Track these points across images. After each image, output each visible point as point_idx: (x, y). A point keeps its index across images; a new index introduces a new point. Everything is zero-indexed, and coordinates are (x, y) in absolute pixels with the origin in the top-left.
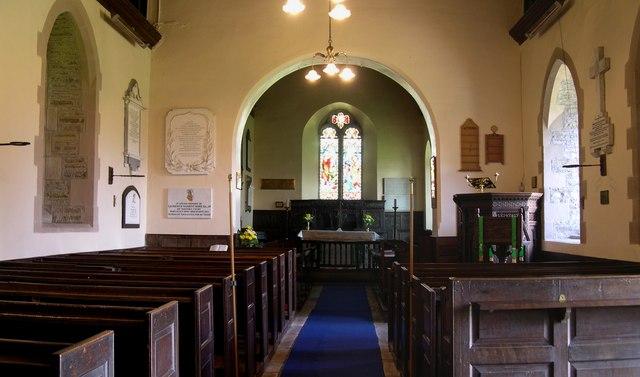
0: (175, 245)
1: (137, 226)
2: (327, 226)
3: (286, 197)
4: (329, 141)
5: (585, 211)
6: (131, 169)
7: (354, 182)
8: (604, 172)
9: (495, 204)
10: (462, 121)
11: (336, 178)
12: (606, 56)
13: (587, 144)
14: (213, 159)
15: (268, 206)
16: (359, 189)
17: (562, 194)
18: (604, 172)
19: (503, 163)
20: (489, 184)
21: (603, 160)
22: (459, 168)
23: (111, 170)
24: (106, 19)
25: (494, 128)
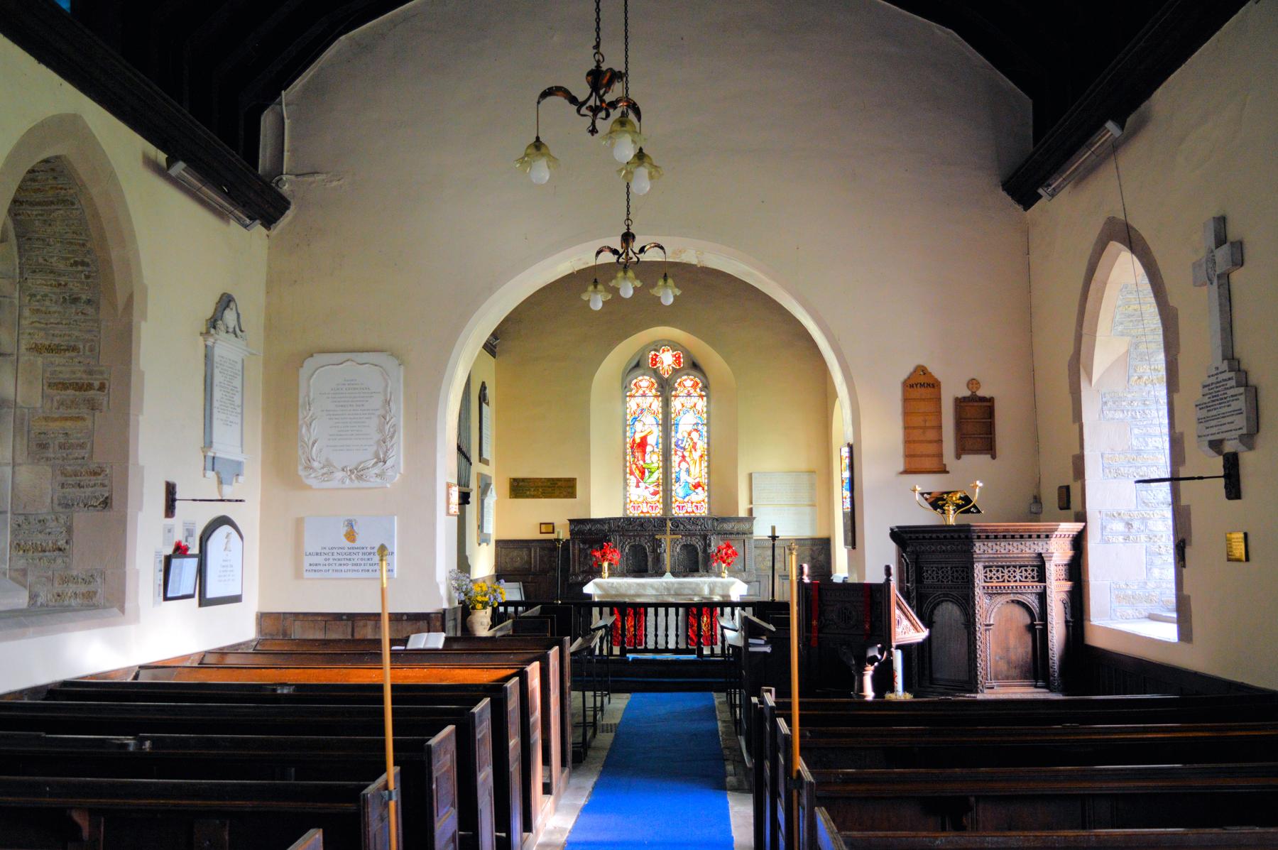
0: (319, 635)
1: (236, 599)
2: (640, 571)
4: (645, 403)
6: (220, 482)
7: (692, 481)
8: (1233, 489)
9: (979, 547)
10: (905, 371)
11: (658, 475)
12: (1232, 236)
13: (1190, 430)
14: (398, 456)
15: (527, 531)
16: (701, 495)
17: (1129, 525)
18: (1233, 489)
19: (994, 457)
20: (966, 505)
22: (901, 468)
23: (171, 490)
24: (162, 172)
25: (973, 383)
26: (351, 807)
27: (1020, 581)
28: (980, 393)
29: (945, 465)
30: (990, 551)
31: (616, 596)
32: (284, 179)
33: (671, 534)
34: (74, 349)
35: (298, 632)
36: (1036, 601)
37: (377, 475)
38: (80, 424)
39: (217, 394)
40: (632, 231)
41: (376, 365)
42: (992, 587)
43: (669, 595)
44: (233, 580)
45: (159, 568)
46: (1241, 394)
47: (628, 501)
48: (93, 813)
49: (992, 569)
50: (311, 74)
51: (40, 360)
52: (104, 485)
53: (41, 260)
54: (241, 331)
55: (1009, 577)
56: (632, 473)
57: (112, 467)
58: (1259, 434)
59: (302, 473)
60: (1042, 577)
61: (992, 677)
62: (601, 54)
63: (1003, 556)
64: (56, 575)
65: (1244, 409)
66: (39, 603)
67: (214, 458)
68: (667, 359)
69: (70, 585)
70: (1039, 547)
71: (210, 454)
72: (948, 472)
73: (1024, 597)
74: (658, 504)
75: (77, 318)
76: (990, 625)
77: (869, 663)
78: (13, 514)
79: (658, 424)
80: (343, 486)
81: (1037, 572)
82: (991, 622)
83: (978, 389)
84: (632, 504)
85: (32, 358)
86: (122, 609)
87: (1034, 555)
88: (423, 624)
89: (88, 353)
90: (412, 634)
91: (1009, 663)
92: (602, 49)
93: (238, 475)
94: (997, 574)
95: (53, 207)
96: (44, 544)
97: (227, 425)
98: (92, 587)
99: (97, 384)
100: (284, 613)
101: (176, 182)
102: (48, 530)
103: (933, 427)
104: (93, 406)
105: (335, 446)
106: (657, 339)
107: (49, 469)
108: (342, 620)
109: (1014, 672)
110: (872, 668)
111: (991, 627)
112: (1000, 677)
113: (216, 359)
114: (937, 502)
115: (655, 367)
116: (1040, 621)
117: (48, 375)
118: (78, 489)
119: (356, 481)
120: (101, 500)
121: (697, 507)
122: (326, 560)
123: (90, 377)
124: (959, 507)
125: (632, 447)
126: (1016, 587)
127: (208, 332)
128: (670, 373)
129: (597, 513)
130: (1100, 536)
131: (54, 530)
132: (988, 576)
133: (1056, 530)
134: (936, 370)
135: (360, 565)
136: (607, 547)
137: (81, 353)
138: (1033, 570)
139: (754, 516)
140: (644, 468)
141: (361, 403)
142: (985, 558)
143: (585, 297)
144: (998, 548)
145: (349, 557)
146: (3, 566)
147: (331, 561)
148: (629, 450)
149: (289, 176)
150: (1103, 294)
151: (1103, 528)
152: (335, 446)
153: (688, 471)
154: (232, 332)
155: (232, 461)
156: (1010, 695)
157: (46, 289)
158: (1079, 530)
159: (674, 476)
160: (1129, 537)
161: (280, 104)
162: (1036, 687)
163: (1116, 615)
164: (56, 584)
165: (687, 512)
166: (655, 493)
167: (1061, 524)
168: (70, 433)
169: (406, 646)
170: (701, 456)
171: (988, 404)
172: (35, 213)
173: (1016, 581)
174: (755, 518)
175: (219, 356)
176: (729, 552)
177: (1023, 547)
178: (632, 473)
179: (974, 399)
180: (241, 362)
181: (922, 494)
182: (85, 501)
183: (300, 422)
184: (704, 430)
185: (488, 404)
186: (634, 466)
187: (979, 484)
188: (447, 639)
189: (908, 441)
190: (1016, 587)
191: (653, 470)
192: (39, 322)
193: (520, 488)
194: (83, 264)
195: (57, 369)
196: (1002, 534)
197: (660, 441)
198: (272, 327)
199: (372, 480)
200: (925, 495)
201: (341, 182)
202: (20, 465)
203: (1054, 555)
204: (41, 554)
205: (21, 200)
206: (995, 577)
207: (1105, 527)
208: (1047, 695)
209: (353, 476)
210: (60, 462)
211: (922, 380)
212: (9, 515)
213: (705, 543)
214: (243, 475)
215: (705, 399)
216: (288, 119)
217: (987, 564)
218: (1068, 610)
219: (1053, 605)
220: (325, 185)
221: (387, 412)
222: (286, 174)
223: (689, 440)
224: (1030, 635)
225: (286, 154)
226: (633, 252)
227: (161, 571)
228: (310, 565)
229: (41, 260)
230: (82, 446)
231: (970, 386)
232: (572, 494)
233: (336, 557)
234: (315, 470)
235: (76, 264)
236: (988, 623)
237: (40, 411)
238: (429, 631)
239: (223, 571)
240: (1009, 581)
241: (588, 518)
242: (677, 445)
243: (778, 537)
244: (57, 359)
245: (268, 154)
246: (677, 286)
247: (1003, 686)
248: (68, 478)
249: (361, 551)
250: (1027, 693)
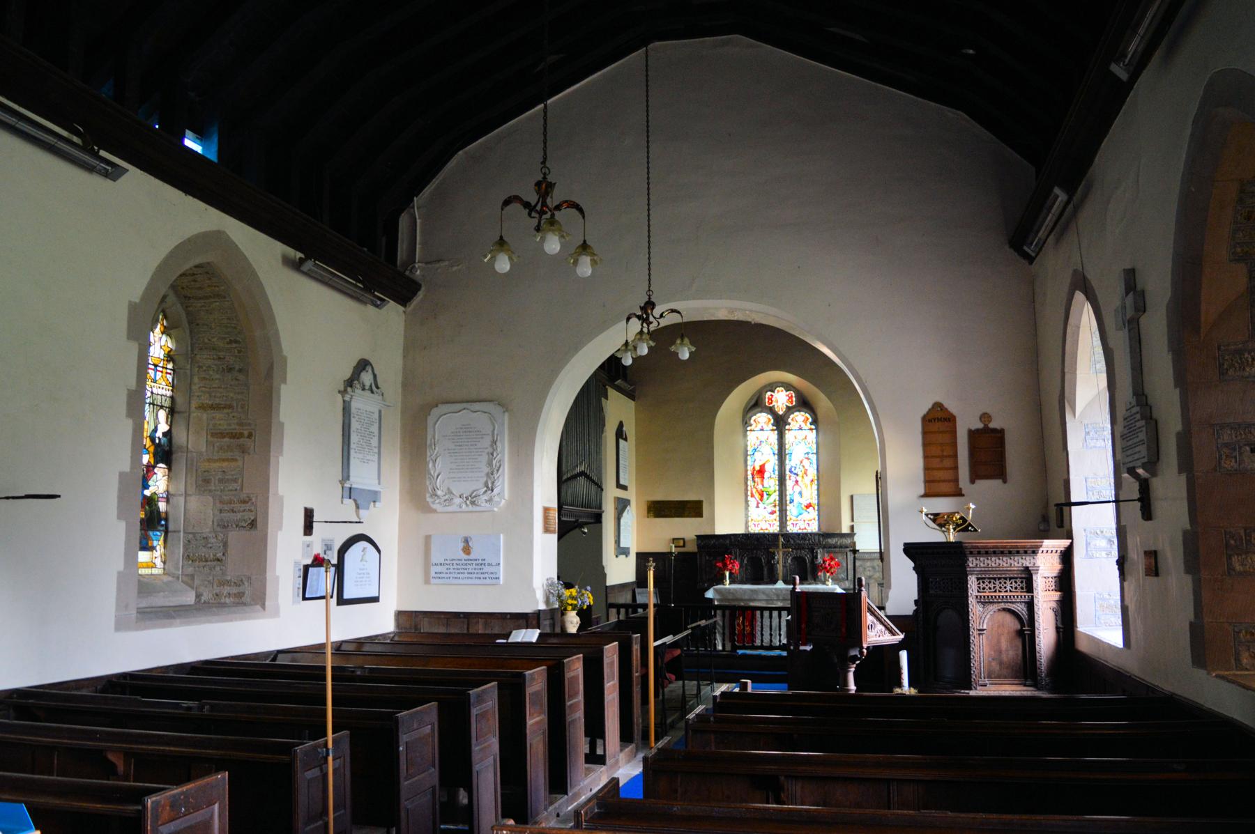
0: (442, 630)
1: (375, 600)
2: (757, 580)
3: (687, 529)
4: (762, 436)
5: (1126, 584)
6: (357, 507)
7: (805, 503)
9: (972, 562)
11: (775, 496)
16: (813, 514)
19: (1005, 482)
21: (1145, 487)
22: (922, 492)
23: (309, 514)
24: (297, 266)
25: (985, 417)
26: (285, 758)
27: (1011, 591)
28: (991, 425)
29: (961, 489)
30: (982, 565)
31: (733, 600)
32: (417, 266)
33: (783, 548)
34: (230, 407)
35: (426, 627)
36: (1025, 609)
37: (486, 501)
38: (233, 464)
39: (354, 438)
40: (653, 299)
41: (485, 412)
42: (984, 596)
43: (778, 600)
44: (370, 585)
45: (298, 575)
46: (1143, 426)
47: (750, 519)
48: (128, 755)
49: (1017, 580)
50: (437, 182)
51: (205, 416)
52: (250, 511)
53: (206, 341)
54: (378, 388)
55: (1000, 588)
56: (752, 496)
57: (257, 496)
58: (1160, 462)
59: (429, 499)
60: (1030, 588)
61: (986, 677)
62: (548, 168)
63: (994, 569)
64: (215, 579)
65: (1146, 440)
66: (203, 601)
67: (350, 488)
68: (781, 399)
69: (225, 587)
70: (1027, 561)
71: (347, 485)
72: (963, 495)
73: (1014, 605)
74: (774, 522)
75: (232, 383)
76: (983, 630)
77: (850, 662)
78: (185, 532)
79: (774, 454)
80: (460, 510)
81: (1026, 583)
82: (985, 627)
83: (990, 421)
84: (753, 522)
85: (199, 414)
86: (263, 606)
87: (1022, 569)
88: (522, 622)
89: (239, 410)
90: (514, 629)
91: (1001, 663)
92: (548, 164)
93: (374, 502)
94: (989, 585)
95: (212, 300)
96: (207, 556)
97: (364, 462)
98: (241, 589)
99: (246, 433)
100: (416, 612)
101: (308, 274)
102: (210, 545)
103: (949, 456)
104: (243, 450)
105: (454, 478)
106: (771, 381)
107: (211, 499)
108: (460, 618)
109: (1005, 672)
110: (855, 665)
111: (985, 632)
112: (993, 676)
113: (353, 410)
114: (938, 519)
115: (771, 405)
116: (1028, 627)
117: (211, 426)
118: (232, 514)
119: (470, 506)
120: (249, 522)
121: (809, 524)
122: (447, 569)
123: (241, 428)
124: (958, 525)
125: (753, 474)
126: (1006, 596)
127: (345, 391)
128: (784, 410)
129: (721, 529)
130: (1085, 552)
131: (214, 545)
132: (982, 587)
133: (1041, 546)
134: (952, 406)
135: (474, 573)
136: (727, 559)
137: (235, 410)
138: (1022, 582)
139: (855, 532)
140: (763, 492)
141: (474, 443)
142: (977, 571)
143: (673, 348)
144: (989, 562)
145: (465, 567)
146: (177, 572)
147: (452, 570)
148: (750, 477)
149: (420, 264)
150: (1078, 337)
151: (1088, 544)
152: (454, 478)
153: (800, 493)
154: (368, 390)
155: (369, 491)
156: (1000, 692)
157: (209, 362)
158: (1066, 546)
159: (788, 498)
160: (1111, 553)
161: (413, 207)
162: (1025, 685)
163: (1101, 623)
164: (215, 587)
165: (762, 529)
166: (773, 513)
167: (1045, 541)
168: (226, 471)
169: (507, 639)
170: (812, 481)
171: (999, 435)
172: (199, 305)
173: (1006, 591)
174: (855, 534)
175: (356, 409)
176: (833, 563)
177: (1012, 561)
178: (752, 496)
179: (986, 431)
180: (378, 413)
181: (927, 515)
182: (237, 523)
183: (428, 459)
184: (814, 458)
185: (626, 439)
186: (754, 490)
187: (972, 506)
188: (541, 635)
189: (927, 469)
190: (1006, 596)
191: (770, 493)
192: (205, 387)
193: (659, 509)
194: (236, 342)
195: (218, 422)
196: (992, 550)
197: (777, 468)
198: (408, 384)
199: (482, 505)
200: (929, 516)
201: (460, 267)
202: (190, 495)
203: (1040, 568)
204: (205, 563)
205: (189, 295)
206: (987, 588)
207: (1090, 544)
208: (1034, 692)
209: (468, 502)
210: (219, 493)
211: (940, 415)
212: (182, 534)
213: (813, 555)
214: (380, 502)
215: (814, 431)
216: (419, 218)
217: (980, 576)
218: (1059, 618)
219: (1040, 613)
220: (448, 270)
221: (494, 450)
222: (419, 262)
223: (801, 467)
224: (1020, 640)
225: (418, 246)
226: (653, 317)
227: (300, 577)
228: (436, 573)
229: (206, 341)
230: (235, 481)
231: (983, 419)
232: (699, 514)
233: (455, 567)
234: (438, 497)
235: (231, 342)
236: (981, 628)
237: (205, 454)
238: (527, 628)
239: (360, 578)
240: (1000, 591)
241: (712, 533)
242: (791, 472)
243: (858, 551)
244: (218, 415)
245: (405, 247)
246: (692, 343)
247: (996, 684)
248: (225, 506)
249: (475, 562)
250: (1016, 691)
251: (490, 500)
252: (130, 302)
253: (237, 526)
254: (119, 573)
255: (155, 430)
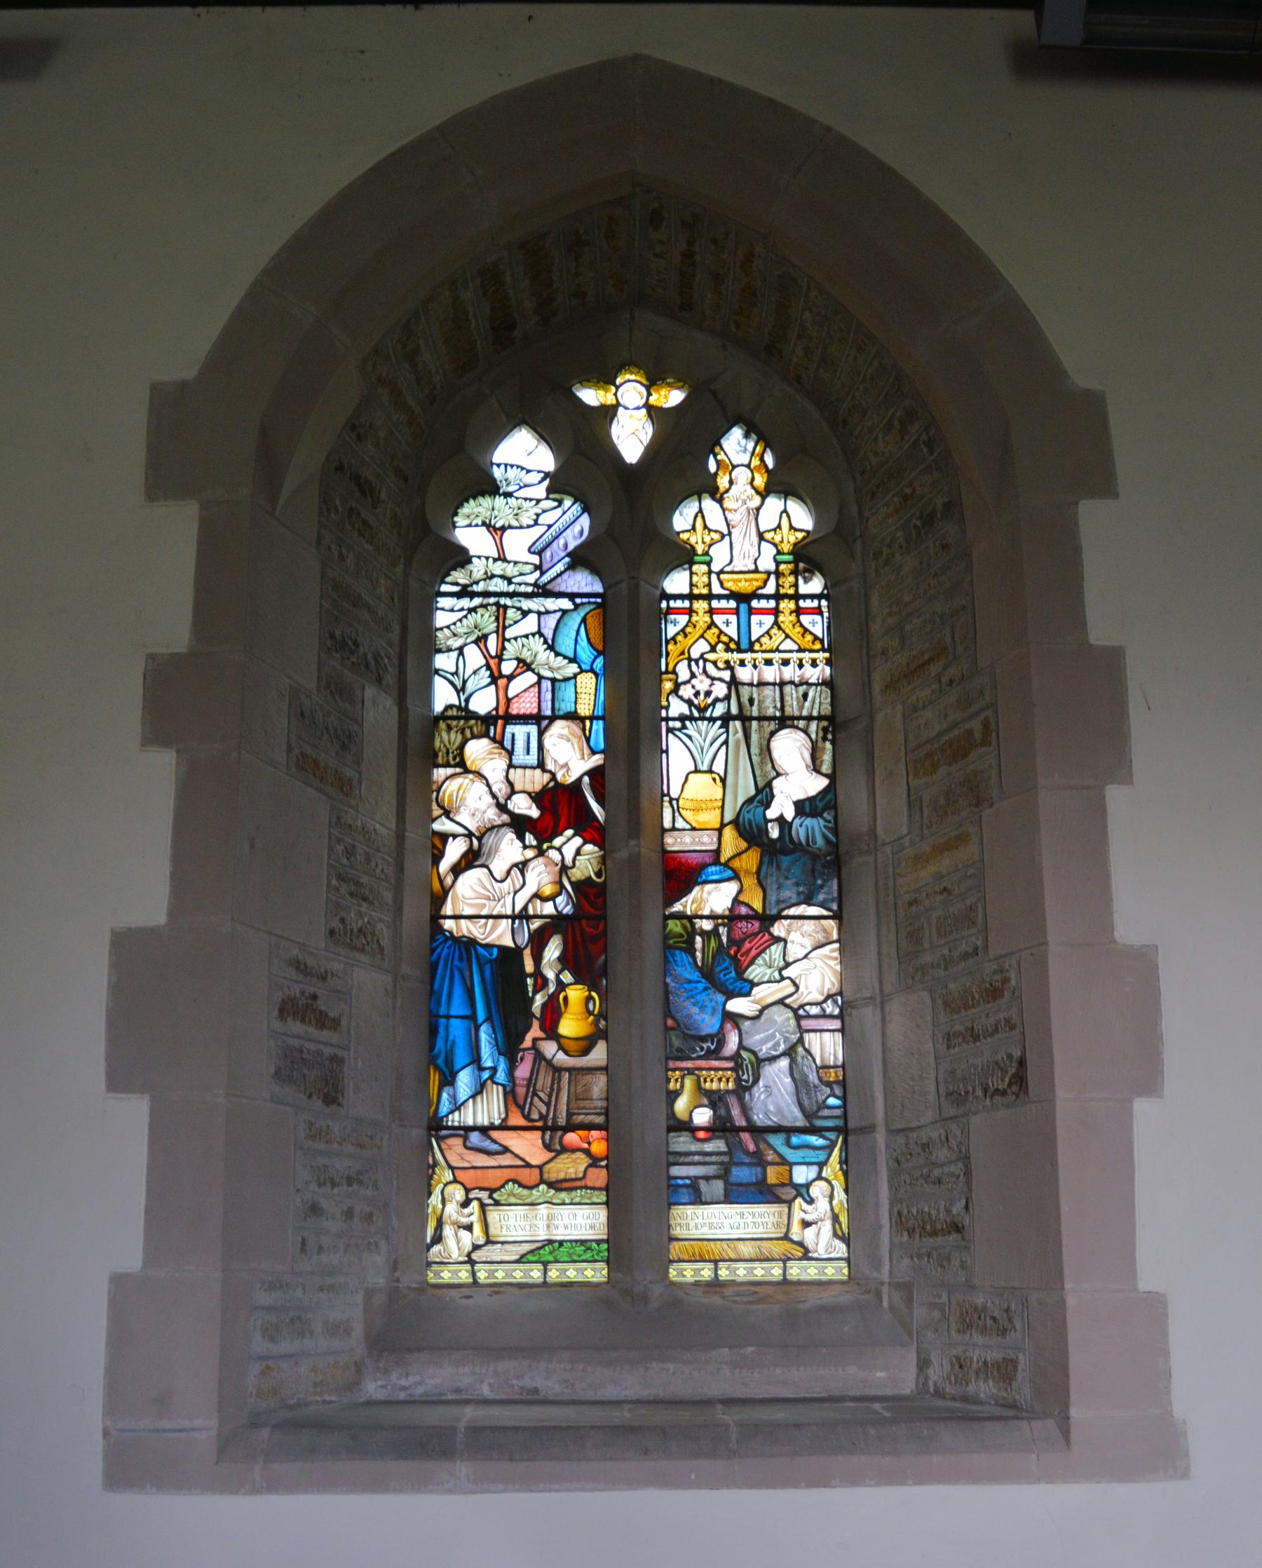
78: (892, 1132)
212: (880, 1137)
251: (891, 670)
252: (157, 390)
253: (985, 1091)
254: (119, 1282)
255: (764, 795)
